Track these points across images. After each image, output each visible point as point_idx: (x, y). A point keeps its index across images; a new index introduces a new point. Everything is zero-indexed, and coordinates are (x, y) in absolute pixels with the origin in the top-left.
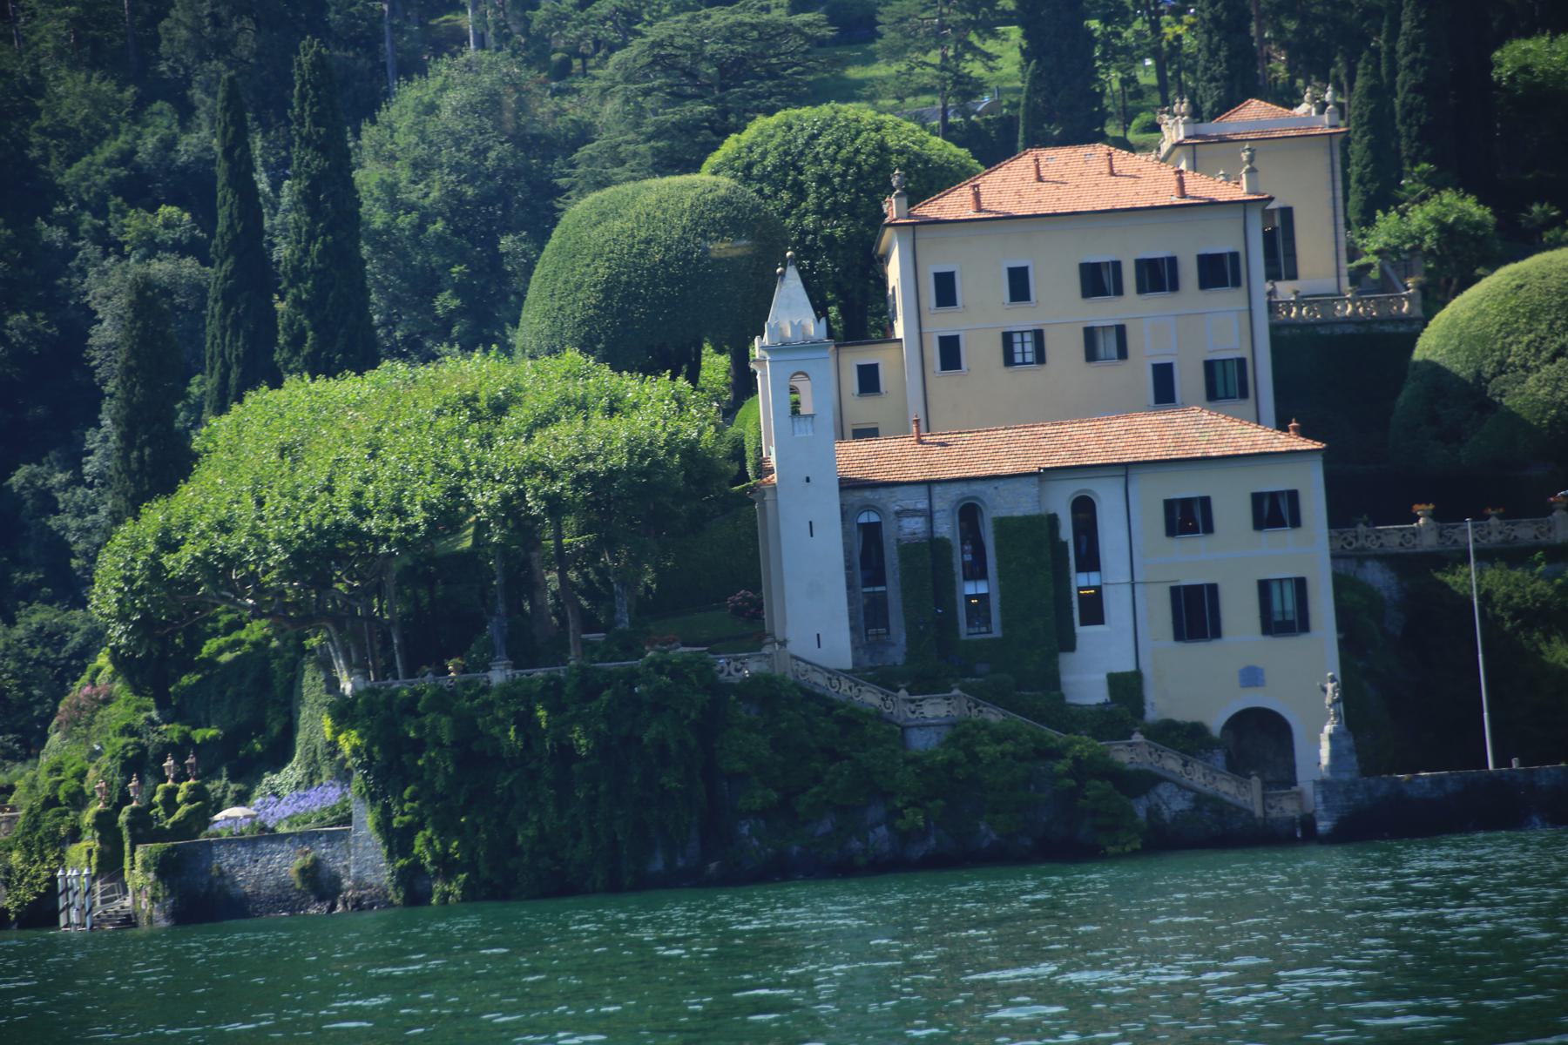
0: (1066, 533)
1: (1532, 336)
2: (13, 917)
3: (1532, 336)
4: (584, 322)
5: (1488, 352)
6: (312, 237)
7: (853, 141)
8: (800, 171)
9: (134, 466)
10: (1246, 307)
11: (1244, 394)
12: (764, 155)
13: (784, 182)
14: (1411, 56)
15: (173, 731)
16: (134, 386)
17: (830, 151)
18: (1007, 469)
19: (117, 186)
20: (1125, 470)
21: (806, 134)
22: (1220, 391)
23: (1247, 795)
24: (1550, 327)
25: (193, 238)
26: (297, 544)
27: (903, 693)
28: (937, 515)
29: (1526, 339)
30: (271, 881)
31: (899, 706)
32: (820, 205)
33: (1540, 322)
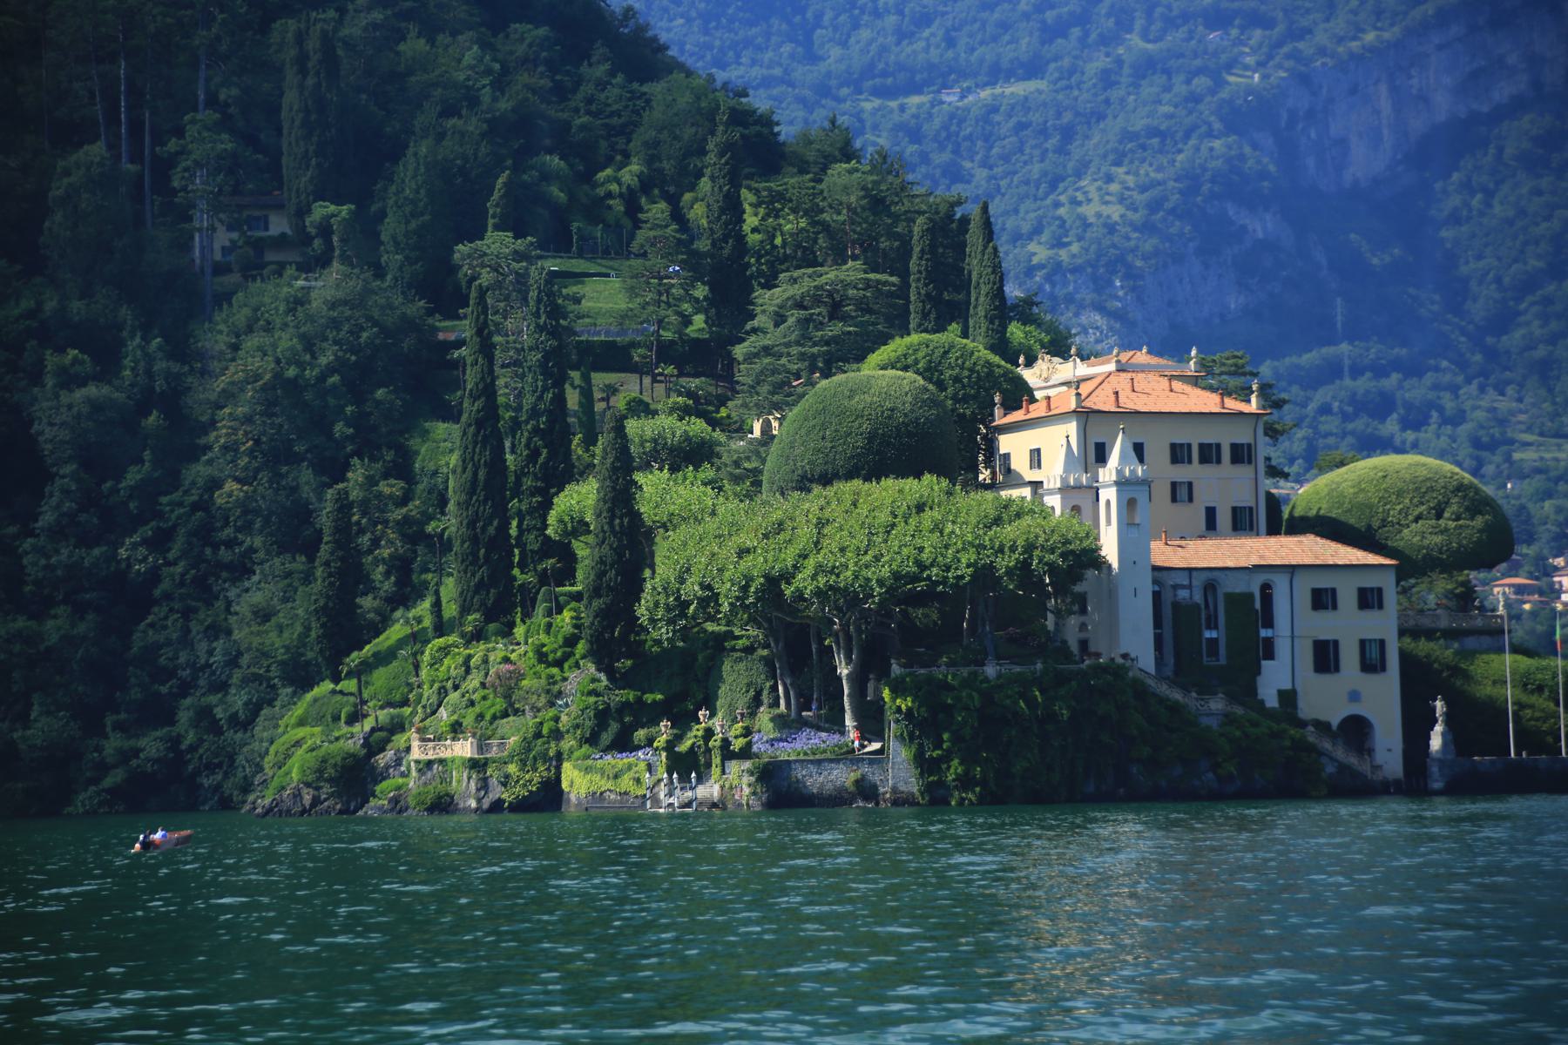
0: (1258, 605)
6: (545, 389)
9: (617, 528)
15: (631, 695)
16: (618, 479)
17: (960, 362)
18: (1230, 564)
20: (1292, 570)
29: (1398, 507)
30: (830, 786)
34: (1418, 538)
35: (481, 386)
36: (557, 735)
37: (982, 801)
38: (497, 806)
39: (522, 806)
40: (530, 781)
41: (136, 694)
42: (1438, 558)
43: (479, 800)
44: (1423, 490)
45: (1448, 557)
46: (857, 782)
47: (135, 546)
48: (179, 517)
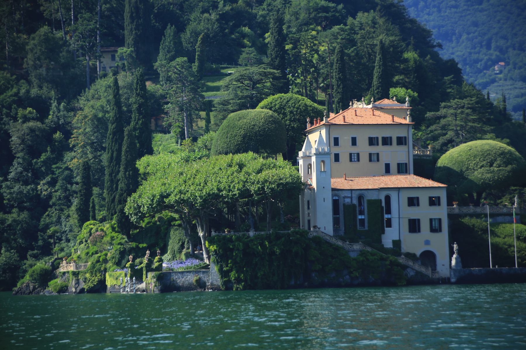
0: (383, 204)
1: (475, 162)
2: (86, 290)
3: (475, 162)
4: (237, 145)
5: (463, 165)
6: (139, 119)
7: (298, 103)
8: (285, 109)
9: (127, 176)
10: (407, 150)
12: (275, 105)
13: (281, 112)
14: (377, 90)
15: (134, 245)
16: (128, 155)
18: (370, 187)
19: (14, 102)
20: (399, 189)
21: (286, 100)
22: (401, 171)
23: (427, 271)
24: (480, 160)
25: (37, 116)
26: (204, 197)
27: (348, 243)
28: (353, 198)
29: (474, 162)
30: (187, 283)
31: (347, 245)
32: (291, 118)
33: (477, 158)
34: (480, 175)
35: (114, 119)
36: (106, 261)
37: (245, 288)
38: (82, 291)
39: (91, 291)
40: (94, 280)
41: (40, 243)
42: (488, 183)
43: (76, 288)
44: (485, 155)
45: (493, 183)
46: (197, 281)
47: (44, 184)
48: (59, 173)
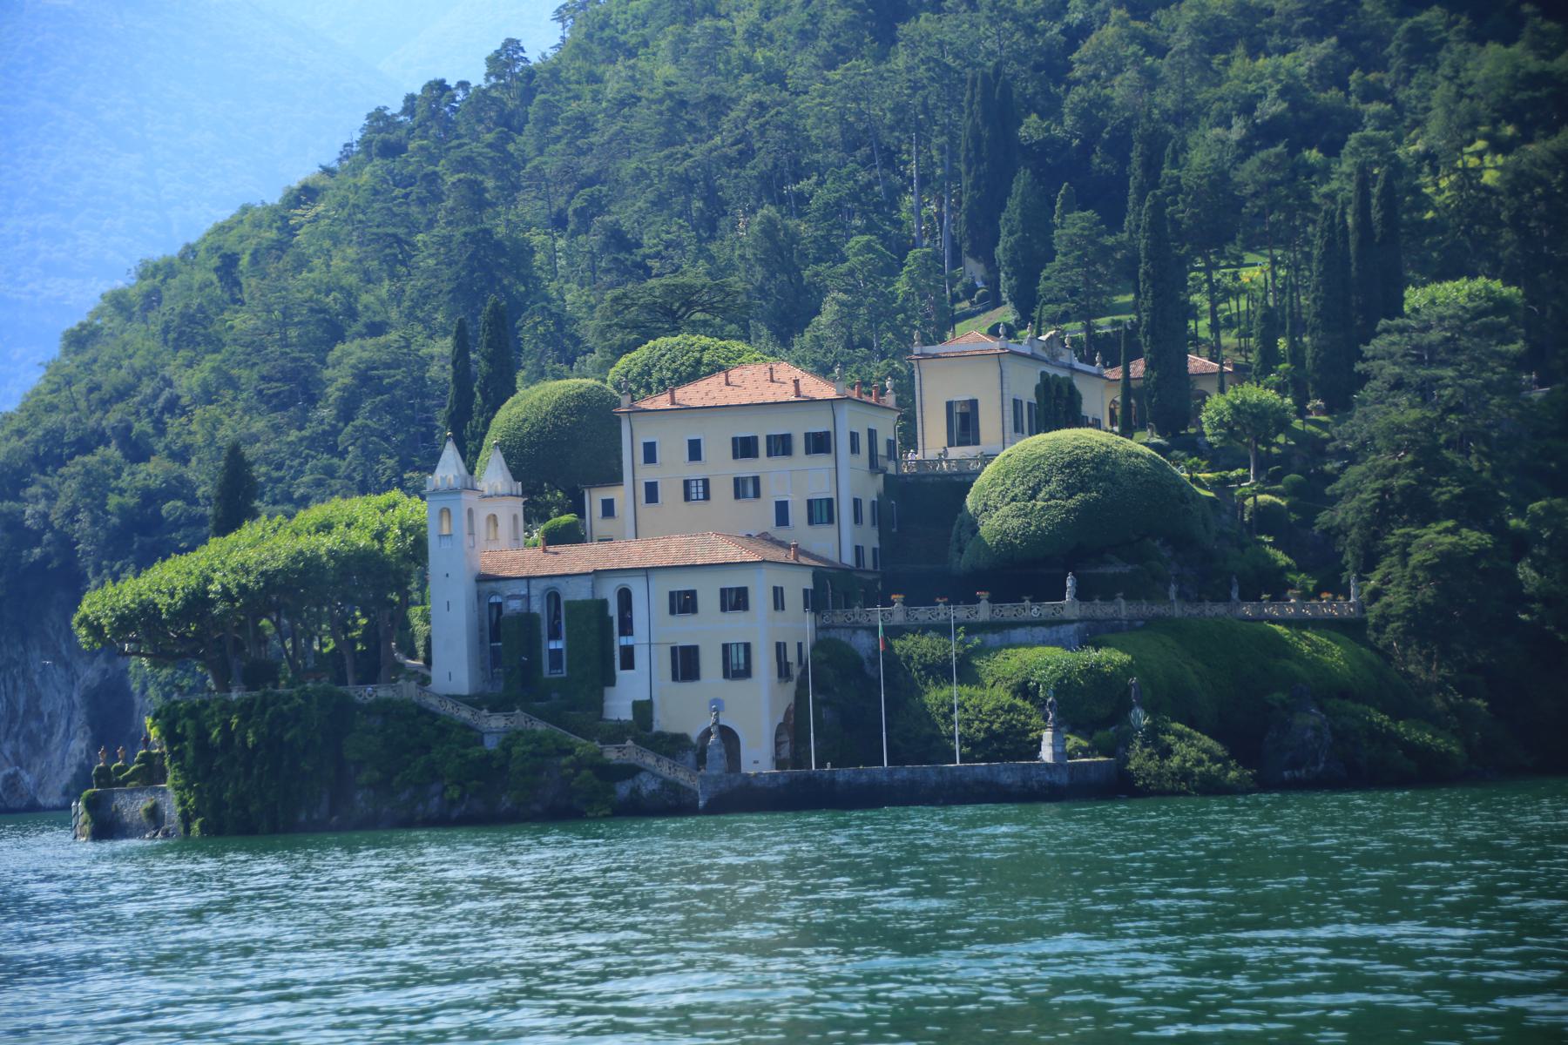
0: (613, 611)
11: (830, 521)
20: (647, 572)
45: (1022, 542)
